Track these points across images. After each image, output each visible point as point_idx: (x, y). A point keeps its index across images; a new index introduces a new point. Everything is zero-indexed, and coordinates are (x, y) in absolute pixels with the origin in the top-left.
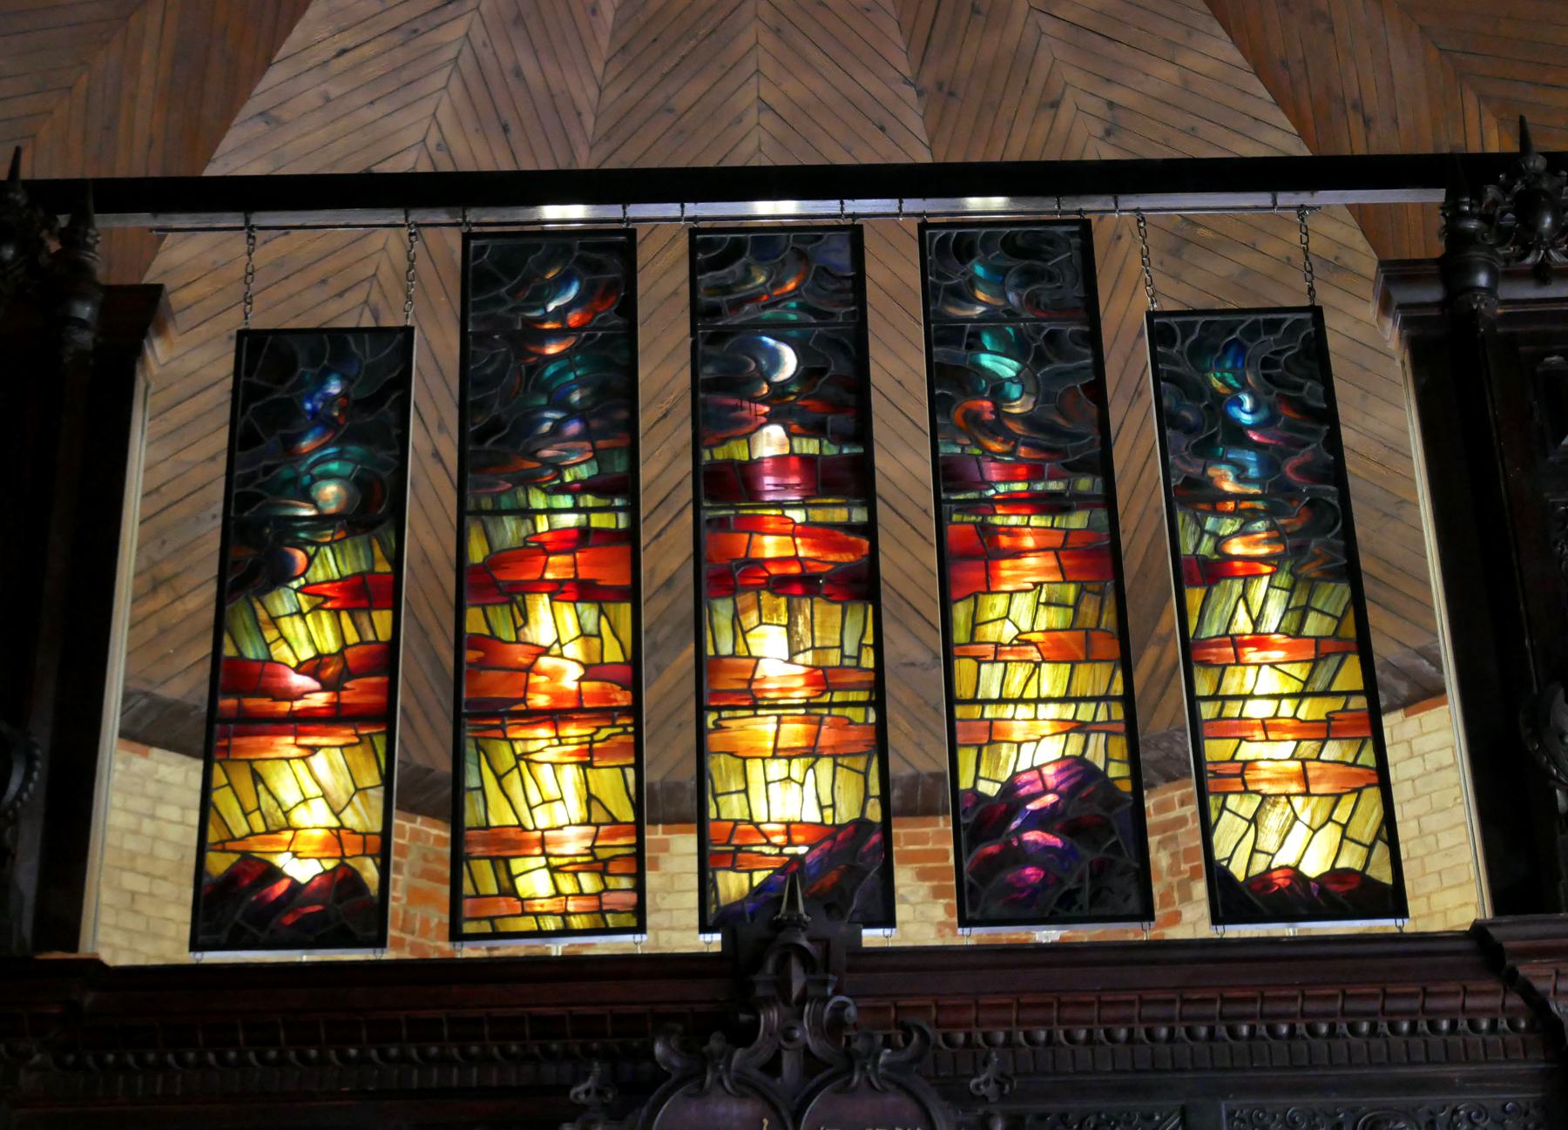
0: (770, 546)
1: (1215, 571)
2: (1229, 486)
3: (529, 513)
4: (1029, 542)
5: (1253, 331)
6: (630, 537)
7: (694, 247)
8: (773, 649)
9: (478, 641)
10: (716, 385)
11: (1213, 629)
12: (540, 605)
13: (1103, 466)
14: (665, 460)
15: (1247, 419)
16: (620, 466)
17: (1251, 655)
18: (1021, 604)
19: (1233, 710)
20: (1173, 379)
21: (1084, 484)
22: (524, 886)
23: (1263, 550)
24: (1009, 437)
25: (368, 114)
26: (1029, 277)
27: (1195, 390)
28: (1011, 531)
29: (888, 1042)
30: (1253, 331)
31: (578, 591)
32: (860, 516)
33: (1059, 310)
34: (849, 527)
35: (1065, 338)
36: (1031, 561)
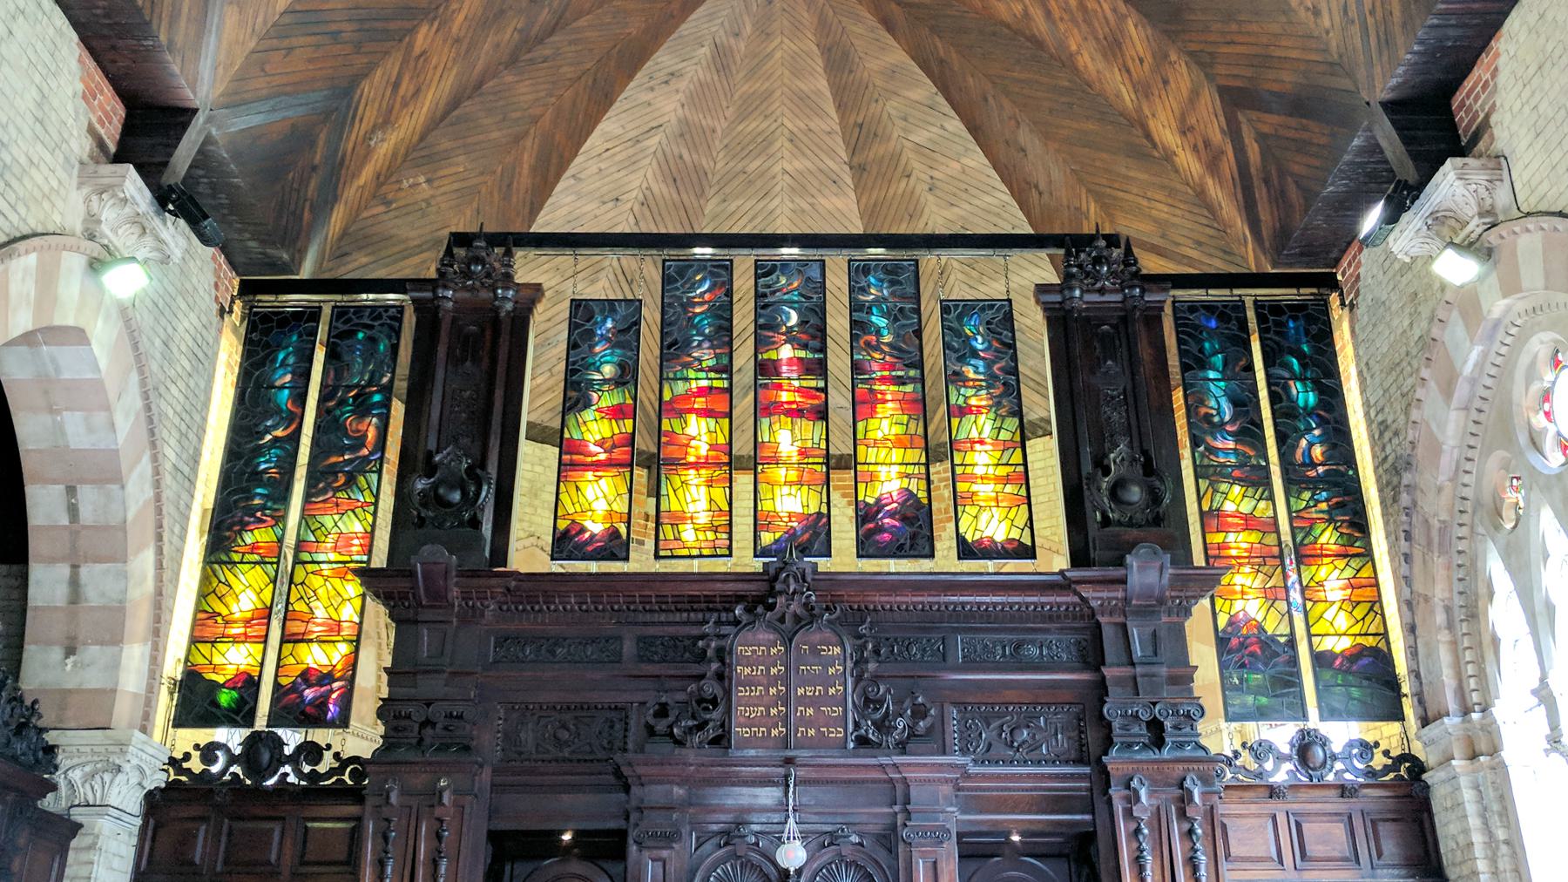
0: (785, 396)
1: (964, 411)
2: (971, 375)
3: (687, 379)
4: (889, 397)
5: (983, 309)
6: (730, 390)
7: (757, 267)
8: (786, 438)
9: (667, 434)
10: (762, 327)
11: (962, 436)
12: (692, 418)
13: (920, 365)
14: (743, 357)
15: (980, 347)
16: (725, 361)
17: (977, 446)
18: (887, 422)
19: (969, 470)
20: (950, 329)
21: (912, 373)
22: (684, 536)
23: (984, 403)
24: (882, 351)
25: (617, 176)
26: (892, 283)
27: (958, 334)
28: (883, 393)
29: (828, 609)
30: (983, 309)
31: (706, 413)
32: (821, 384)
33: (903, 297)
34: (817, 389)
35: (907, 314)
36: (890, 405)
